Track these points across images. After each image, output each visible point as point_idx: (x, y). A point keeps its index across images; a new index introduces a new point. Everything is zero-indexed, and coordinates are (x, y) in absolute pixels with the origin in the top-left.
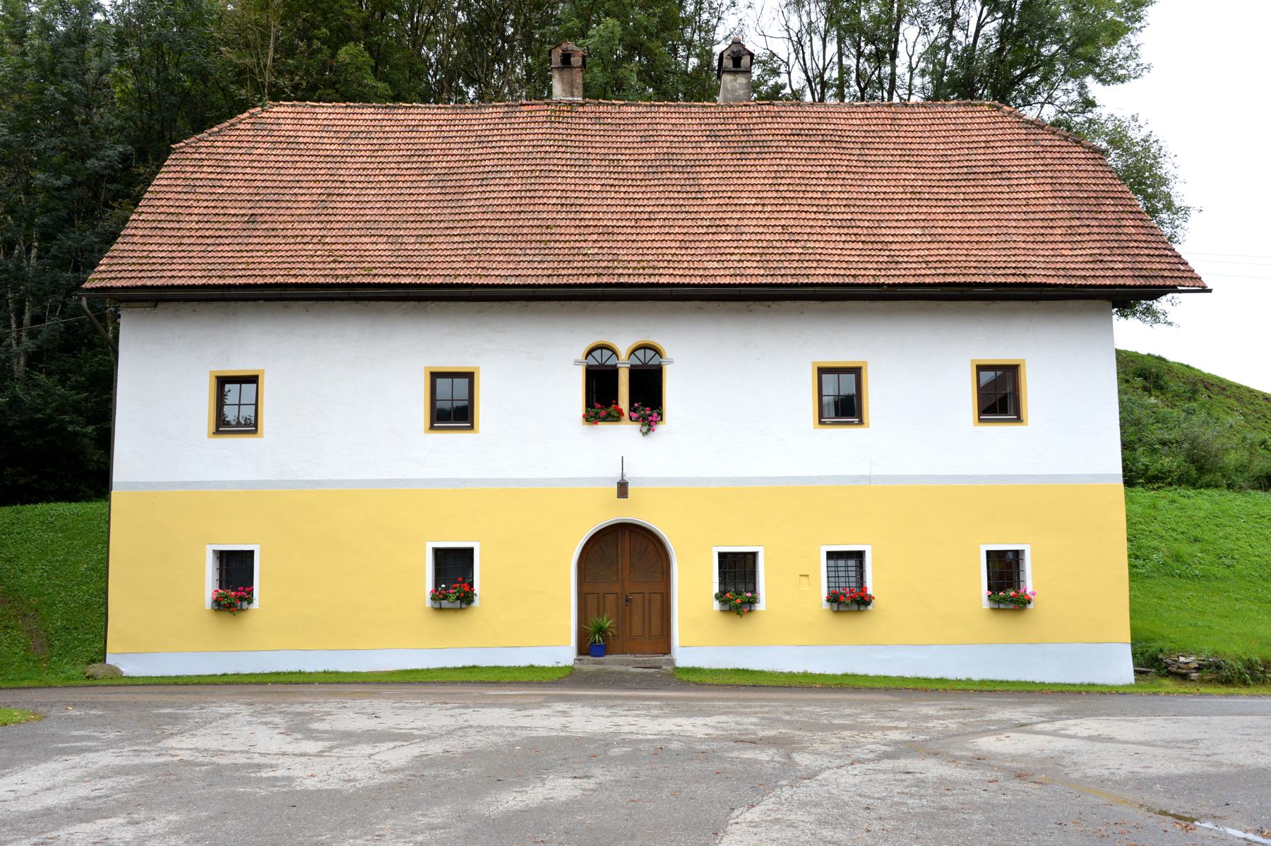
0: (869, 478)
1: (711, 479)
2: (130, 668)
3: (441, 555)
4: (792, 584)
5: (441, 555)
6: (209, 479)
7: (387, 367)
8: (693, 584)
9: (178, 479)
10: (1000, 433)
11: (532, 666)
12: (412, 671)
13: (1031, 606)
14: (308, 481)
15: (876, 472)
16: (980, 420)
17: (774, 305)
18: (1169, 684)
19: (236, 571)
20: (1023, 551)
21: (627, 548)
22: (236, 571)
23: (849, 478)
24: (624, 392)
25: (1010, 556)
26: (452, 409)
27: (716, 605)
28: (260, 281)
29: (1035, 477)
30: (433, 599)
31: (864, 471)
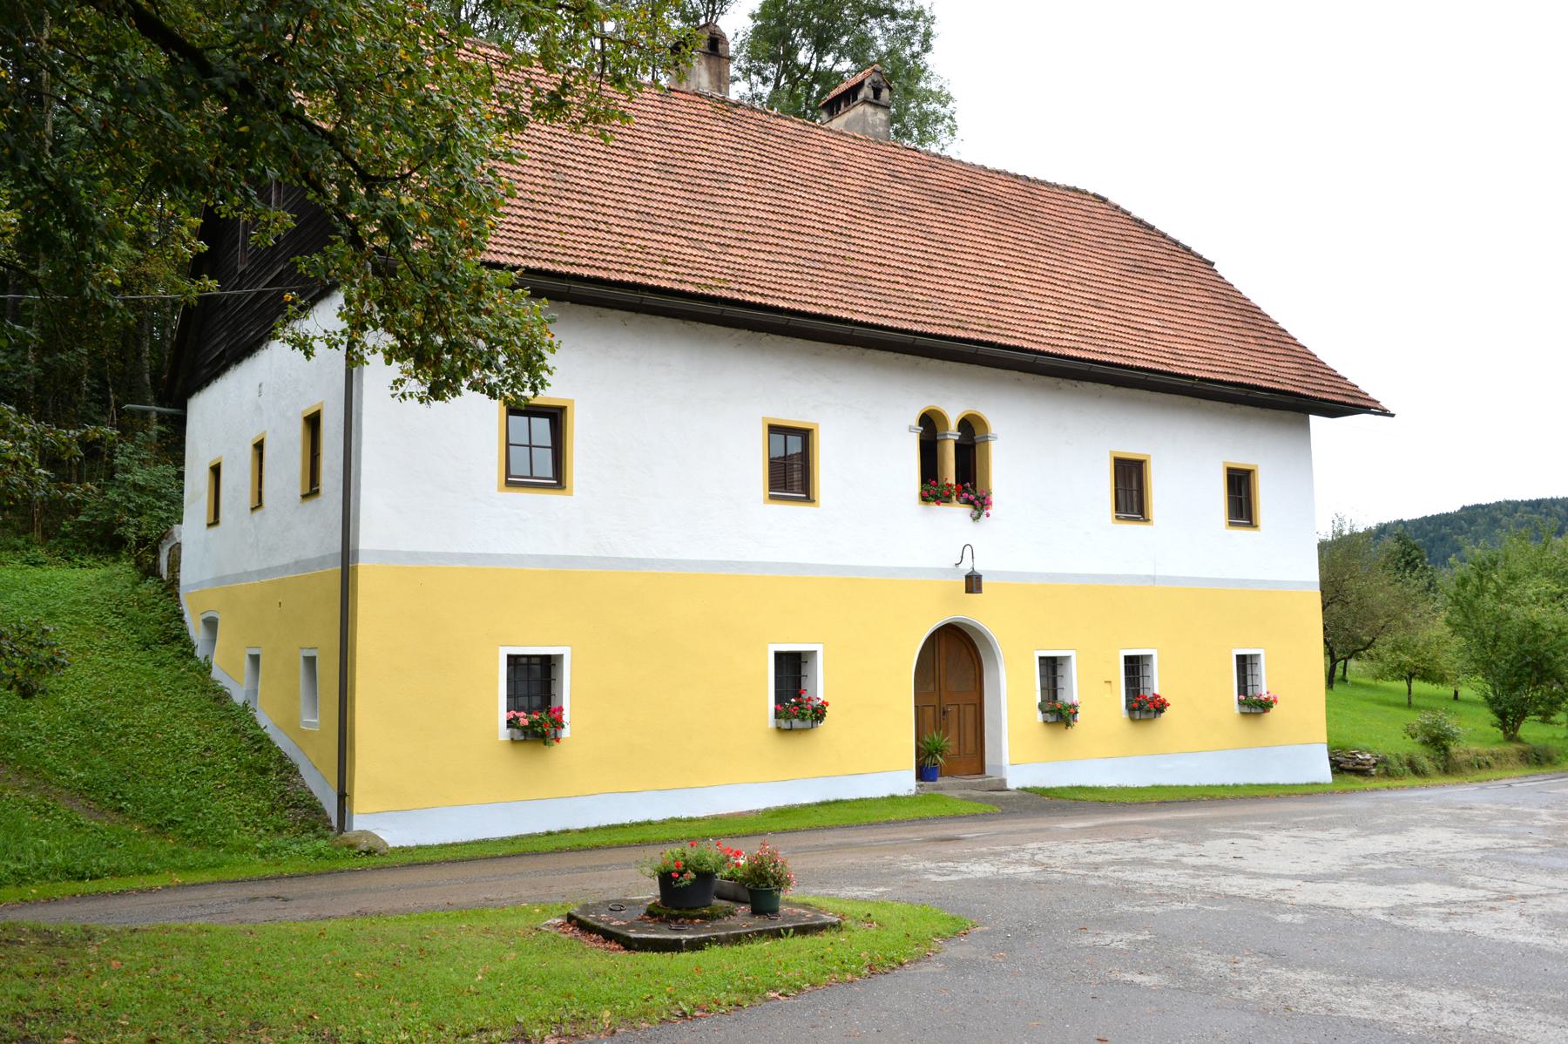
0: (1153, 579)
1: (1032, 575)
2: (395, 834)
3: (1128, 659)
4: (1096, 690)
5: (1128, 659)
6: (500, 551)
7: (719, 407)
8: (1012, 694)
9: (456, 550)
10: (791, 513)
11: (893, 797)
12: (1268, 786)
13: (1168, 711)
14: (631, 560)
15: (1160, 572)
16: (772, 497)
17: (1064, 383)
18: (1360, 782)
19: (534, 681)
20: (560, 657)
21: (943, 650)
22: (534, 681)
23: (1139, 577)
24: (954, 468)
25: (524, 660)
26: (791, 472)
27: (1039, 716)
28: (614, 276)
29: (1265, 582)
30: (777, 715)
31: (1147, 570)
